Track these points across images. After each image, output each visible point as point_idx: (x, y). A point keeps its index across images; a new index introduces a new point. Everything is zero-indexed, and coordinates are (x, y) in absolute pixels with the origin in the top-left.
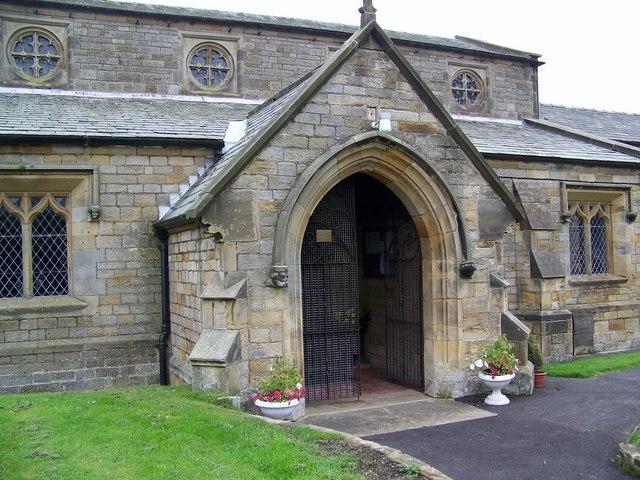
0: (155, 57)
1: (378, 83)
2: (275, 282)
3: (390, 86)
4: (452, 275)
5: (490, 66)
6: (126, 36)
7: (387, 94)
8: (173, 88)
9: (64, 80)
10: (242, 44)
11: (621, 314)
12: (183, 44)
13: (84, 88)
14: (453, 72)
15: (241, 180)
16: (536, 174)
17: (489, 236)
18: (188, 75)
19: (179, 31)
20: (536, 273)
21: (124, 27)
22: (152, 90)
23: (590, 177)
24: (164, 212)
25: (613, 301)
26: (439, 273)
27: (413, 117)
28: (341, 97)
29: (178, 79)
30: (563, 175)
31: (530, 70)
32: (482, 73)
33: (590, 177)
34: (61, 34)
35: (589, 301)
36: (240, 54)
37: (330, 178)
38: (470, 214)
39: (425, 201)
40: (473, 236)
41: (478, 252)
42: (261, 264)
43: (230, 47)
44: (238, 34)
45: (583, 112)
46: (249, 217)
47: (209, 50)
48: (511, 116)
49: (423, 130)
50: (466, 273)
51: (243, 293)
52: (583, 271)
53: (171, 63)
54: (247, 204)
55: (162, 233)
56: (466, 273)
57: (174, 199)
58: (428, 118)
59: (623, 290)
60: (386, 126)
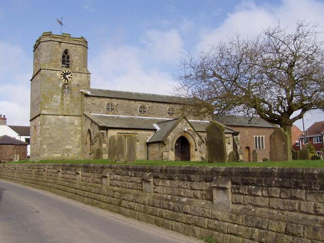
0: (133, 108)
1: (184, 124)
3: (186, 124)
4: (194, 150)
6: (127, 104)
7: (186, 126)
9: (116, 113)
17: (200, 145)
19: (137, 102)
20: (73, 124)
21: (127, 102)
22: (132, 115)
24: (148, 141)
26: (192, 150)
27: (189, 128)
28: (180, 125)
34: (115, 103)
37: (179, 136)
38: (197, 142)
39: (191, 140)
40: (197, 145)
41: (198, 147)
42: (170, 148)
43: (147, 106)
47: (143, 107)
49: (190, 130)
50: (196, 150)
53: (136, 110)
54: (169, 140)
55: (148, 144)
56: (196, 150)
57: (149, 139)
58: (191, 128)
60: (186, 130)
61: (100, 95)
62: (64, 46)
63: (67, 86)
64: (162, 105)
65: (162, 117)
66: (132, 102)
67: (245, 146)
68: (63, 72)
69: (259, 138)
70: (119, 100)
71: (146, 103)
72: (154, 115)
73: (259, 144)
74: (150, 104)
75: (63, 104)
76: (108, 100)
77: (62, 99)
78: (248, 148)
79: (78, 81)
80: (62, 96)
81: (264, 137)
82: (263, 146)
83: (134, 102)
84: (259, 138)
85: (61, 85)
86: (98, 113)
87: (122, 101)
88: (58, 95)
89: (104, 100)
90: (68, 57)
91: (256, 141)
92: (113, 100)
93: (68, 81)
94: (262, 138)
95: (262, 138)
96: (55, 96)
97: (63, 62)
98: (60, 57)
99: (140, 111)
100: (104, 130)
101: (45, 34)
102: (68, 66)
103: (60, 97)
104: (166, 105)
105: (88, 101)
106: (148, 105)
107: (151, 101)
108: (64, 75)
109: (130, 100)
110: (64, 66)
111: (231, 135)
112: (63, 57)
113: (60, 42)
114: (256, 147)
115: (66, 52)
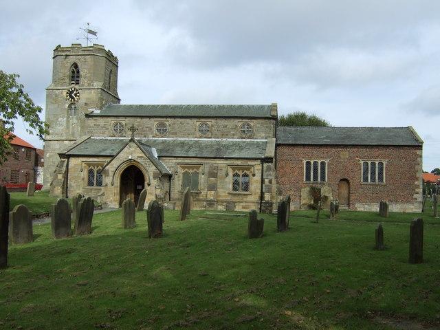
19: (153, 120)
21: (139, 120)
61: (142, 115)
62: (72, 59)
63: (73, 106)
64: (188, 120)
66: (145, 120)
68: (69, 91)
70: (128, 119)
71: (164, 119)
74: (171, 121)
75: (68, 128)
76: (113, 119)
77: (68, 122)
79: (87, 99)
80: (68, 118)
81: (384, 163)
82: (381, 178)
85: (67, 105)
87: (132, 119)
89: (109, 119)
90: (78, 72)
92: (121, 119)
93: (74, 100)
94: (323, 163)
95: (323, 163)
99: (159, 131)
100: (65, 158)
103: (65, 119)
104: (195, 120)
105: (91, 122)
106: (168, 122)
107: (171, 117)
108: (70, 93)
109: (142, 117)
110: (74, 82)
111: (259, 162)
113: (67, 55)
114: (366, 179)
115: (76, 65)
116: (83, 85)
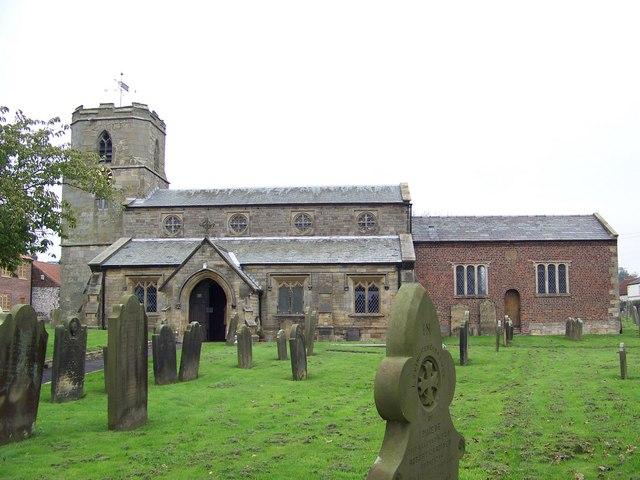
2: (178, 307)
5: (379, 209)
8: (222, 234)
10: (251, 214)
11: (381, 331)
12: (227, 215)
13: (188, 237)
14: (357, 214)
15: (170, 282)
16: (332, 270)
18: (229, 229)
23: (364, 270)
25: (374, 325)
27: (219, 263)
29: (224, 231)
30: (347, 270)
31: (406, 208)
32: (375, 213)
33: (364, 270)
34: (181, 217)
35: (358, 325)
36: (251, 218)
43: (247, 215)
44: (249, 210)
45: (471, 218)
46: (171, 291)
47: (238, 218)
48: (392, 234)
49: (222, 266)
51: (169, 309)
52: (363, 310)
53: (221, 224)
58: (224, 263)
59: (382, 320)
62: (100, 126)
65: (279, 235)
66: (213, 212)
67: (505, 287)
69: (551, 267)
72: (259, 231)
73: (552, 281)
74: (186, 212)
75: (96, 227)
77: (96, 217)
78: (513, 293)
82: (563, 288)
83: (218, 210)
84: (551, 267)
86: (147, 237)
88: (88, 211)
89: (159, 212)
90: (110, 144)
91: (541, 275)
94: (562, 267)
95: (562, 267)
96: (84, 214)
97: (102, 153)
98: (95, 146)
101: (103, 107)
102: (109, 160)
103: (91, 214)
104: (289, 210)
112: (102, 144)
114: (542, 289)
115: (106, 135)
116: (117, 163)
